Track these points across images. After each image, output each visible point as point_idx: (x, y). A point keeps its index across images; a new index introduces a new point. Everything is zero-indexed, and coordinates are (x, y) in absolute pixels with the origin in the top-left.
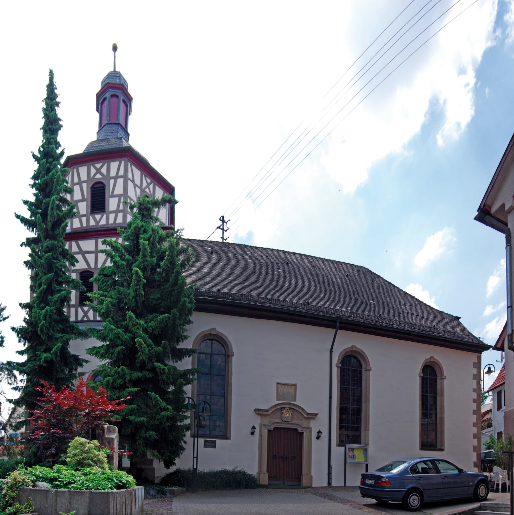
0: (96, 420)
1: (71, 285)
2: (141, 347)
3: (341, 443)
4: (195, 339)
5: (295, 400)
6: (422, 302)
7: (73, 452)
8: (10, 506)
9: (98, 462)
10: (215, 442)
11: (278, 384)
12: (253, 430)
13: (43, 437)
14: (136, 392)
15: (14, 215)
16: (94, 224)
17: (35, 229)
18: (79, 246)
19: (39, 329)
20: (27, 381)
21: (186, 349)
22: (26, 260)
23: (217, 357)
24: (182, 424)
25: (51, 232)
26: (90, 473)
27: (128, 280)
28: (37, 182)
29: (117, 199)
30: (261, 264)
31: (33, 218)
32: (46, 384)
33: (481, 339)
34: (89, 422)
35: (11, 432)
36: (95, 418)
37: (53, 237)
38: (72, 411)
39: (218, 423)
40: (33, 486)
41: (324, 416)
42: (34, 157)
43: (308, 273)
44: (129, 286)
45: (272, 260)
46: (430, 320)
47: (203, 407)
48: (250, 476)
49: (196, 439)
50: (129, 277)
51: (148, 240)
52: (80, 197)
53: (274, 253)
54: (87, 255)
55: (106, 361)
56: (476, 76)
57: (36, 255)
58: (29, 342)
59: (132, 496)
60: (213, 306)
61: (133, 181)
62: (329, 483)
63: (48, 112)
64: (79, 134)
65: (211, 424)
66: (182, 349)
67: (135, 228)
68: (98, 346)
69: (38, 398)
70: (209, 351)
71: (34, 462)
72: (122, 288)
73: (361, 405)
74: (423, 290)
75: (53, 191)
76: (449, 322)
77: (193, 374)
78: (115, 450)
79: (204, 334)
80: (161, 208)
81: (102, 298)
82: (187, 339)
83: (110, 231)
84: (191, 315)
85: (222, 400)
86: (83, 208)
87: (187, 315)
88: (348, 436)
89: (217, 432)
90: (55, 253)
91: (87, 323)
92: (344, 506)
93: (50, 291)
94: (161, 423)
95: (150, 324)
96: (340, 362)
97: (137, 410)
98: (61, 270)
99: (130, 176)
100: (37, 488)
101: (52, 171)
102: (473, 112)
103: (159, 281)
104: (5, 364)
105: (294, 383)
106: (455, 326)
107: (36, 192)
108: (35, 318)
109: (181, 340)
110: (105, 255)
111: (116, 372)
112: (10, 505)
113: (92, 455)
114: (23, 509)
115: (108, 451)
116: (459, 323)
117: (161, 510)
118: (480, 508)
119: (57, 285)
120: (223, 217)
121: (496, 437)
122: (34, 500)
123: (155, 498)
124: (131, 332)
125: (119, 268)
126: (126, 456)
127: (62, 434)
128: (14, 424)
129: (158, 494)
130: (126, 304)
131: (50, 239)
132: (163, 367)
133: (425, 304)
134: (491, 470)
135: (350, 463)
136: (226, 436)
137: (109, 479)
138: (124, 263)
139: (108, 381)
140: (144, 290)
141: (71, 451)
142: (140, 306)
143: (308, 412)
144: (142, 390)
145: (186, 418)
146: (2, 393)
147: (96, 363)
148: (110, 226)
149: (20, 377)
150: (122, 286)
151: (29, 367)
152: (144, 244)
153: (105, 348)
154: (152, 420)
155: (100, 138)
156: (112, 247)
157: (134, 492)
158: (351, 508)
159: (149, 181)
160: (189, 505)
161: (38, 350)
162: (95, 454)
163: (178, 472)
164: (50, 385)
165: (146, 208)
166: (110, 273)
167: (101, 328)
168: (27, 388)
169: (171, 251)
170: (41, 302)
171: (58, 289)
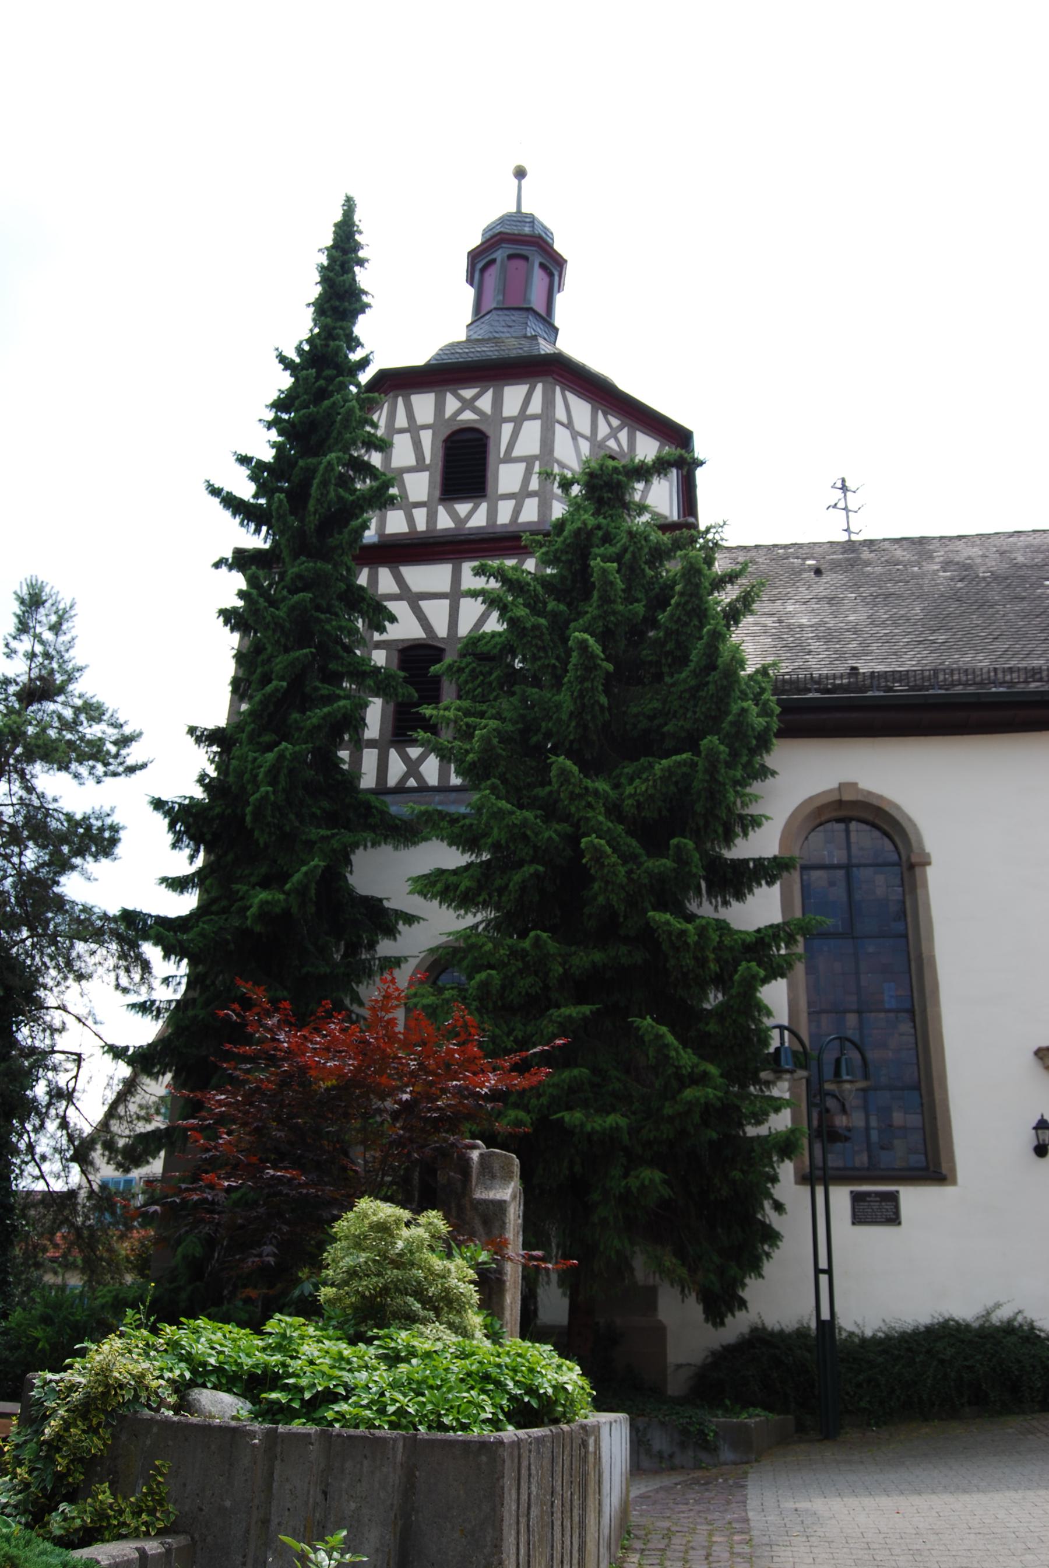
0: (437, 1130)
1: (370, 682)
2: (602, 865)
7: (348, 1262)
9: (443, 1305)
10: (893, 1198)
13: (235, 1196)
14: (585, 1018)
15: (204, 486)
17: (264, 529)
18: (400, 580)
19: (249, 810)
20: (189, 984)
21: (758, 862)
22: (228, 605)
24: (762, 1130)
25: (314, 540)
26: (412, 1353)
27: (554, 666)
28: (285, 416)
29: (522, 466)
30: (984, 578)
31: (262, 501)
34: (411, 1140)
35: (106, 1171)
36: (437, 1124)
38: (352, 1093)
39: (898, 1118)
40: (177, 1409)
44: (557, 684)
45: (1020, 559)
47: (838, 1061)
49: (820, 1190)
50: (558, 658)
51: (618, 558)
52: (412, 461)
54: (424, 604)
55: (479, 917)
58: (208, 852)
61: (569, 425)
63: (331, 274)
64: (417, 314)
65: (874, 1123)
66: (746, 861)
67: (577, 533)
69: (228, 1046)
70: (838, 856)
75: (331, 441)
77: (790, 940)
82: (759, 825)
84: (768, 750)
85: (906, 1027)
86: (419, 486)
87: (754, 752)
91: (415, 796)
93: (297, 695)
95: (629, 790)
98: (338, 641)
99: (560, 414)
100: (194, 1419)
104: (115, 919)
107: (280, 439)
108: (240, 775)
109: (738, 830)
110: (483, 602)
111: (514, 953)
113: (420, 1274)
114: (127, 1518)
115: (483, 1257)
119: (323, 681)
120: (843, 480)
123: (673, 1468)
124: (566, 818)
125: (525, 636)
126: (554, 1277)
127: (305, 1185)
130: (548, 735)
131: (310, 556)
132: (678, 925)
136: (933, 1168)
137: (486, 1378)
139: (485, 985)
140: (607, 692)
141: (341, 1257)
145: (777, 1105)
146: (90, 1022)
147: (440, 924)
148: (498, 530)
150: (537, 682)
151: (202, 934)
152: (604, 571)
159: (615, 422)
162: (430, 1270)
167: (463, 810)
169: (688, 582)
171: (325, 692)
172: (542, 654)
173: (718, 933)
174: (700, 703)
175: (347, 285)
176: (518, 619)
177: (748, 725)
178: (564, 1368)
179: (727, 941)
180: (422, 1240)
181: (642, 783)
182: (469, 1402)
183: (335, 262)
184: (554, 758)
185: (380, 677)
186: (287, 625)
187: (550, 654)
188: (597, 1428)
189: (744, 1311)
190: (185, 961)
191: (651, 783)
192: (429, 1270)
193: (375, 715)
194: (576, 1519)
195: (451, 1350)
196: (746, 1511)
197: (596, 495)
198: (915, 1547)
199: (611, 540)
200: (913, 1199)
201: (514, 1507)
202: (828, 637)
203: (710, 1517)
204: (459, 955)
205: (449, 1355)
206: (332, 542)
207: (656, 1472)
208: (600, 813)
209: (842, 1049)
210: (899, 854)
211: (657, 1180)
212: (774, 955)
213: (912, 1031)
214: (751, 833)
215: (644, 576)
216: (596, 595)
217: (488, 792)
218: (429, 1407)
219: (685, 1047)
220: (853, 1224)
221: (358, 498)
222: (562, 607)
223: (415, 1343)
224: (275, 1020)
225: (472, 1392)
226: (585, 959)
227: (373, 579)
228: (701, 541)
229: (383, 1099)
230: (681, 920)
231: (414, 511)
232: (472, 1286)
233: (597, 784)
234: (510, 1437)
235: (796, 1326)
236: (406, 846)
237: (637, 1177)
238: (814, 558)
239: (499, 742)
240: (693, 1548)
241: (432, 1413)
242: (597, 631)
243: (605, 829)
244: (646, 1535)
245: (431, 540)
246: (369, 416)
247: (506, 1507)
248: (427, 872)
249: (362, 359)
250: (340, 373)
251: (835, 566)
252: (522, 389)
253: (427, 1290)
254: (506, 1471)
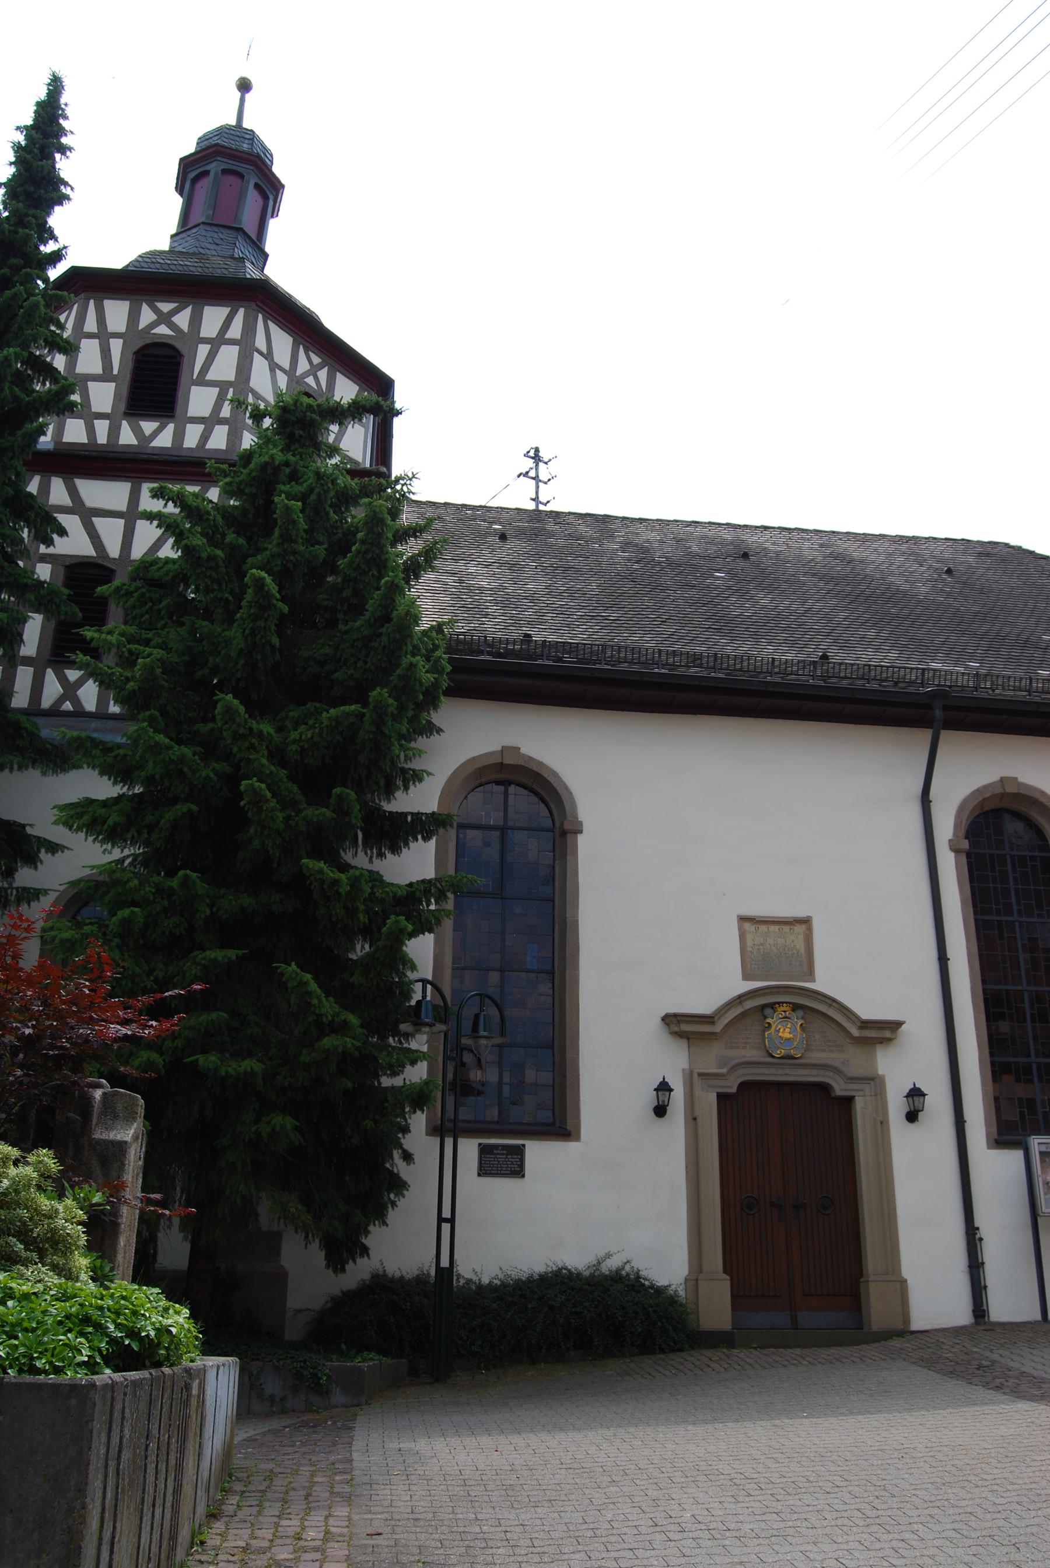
3: (1007, 1133)
5: (810, 975)
9: (49, 1247)
10: (520, 1151)
11: (742, 919)
21: (417, 816)
23: (525, 845)
24: (398, 1081)
27: (227, 601)
30: (660, 563)
39: (530, 1075)
43: (814, 575)
44: (229, 619)
45: (695, 548)
47: (477, 1017)
48: (660, 1291)
49: (449, 1142)
50: (231, 593)
51: (303, 498)
52: (98, 370)
55: (126, 852)
61: (268, 356)
62: (979, 1310)
63: (29, 157)
65: (506, 1079)
66: (404, 815)
67: (264, 467)
68: (102, 797)
70: (495, 818)
77: (441, 897)
78: (128, 1194)
82: (421, 780)
84: (436, 708)
85: (545, 988)
86: (103, 397)
88: (1031, 1104)
95: (294, 735)
96: (962, 833)
99: (260, 342)
101: (14, 286)
105: (802, 913)
109: (399, 783)
110: (159, 526)
113: (25, 1214)
115: (97, 1198)
120: (537, 450)
123: (284, 1412)
126: (176, 1221)
130: (215, 671)
132: (331, 874)
136: (560, 1125)
137: (86, 1320)
138: (219, 552)
139: (127, 923)
140: (280, 633)
145: (413, 1057)
147: (84, 856)
150: (208, 615)
152: (288, 508)
155: (180, 249)
159: (316, 360)
162: (37, 1211)
167: (120, 739)
172: (215, 587)
173: (370, 884)
174: (372, 653)
175: (46, 171)
176: (194, 548)
177: (415, 680)
178: (171, 1311)
179: (378, 893)
180: (31, 1179)
181: (308, 730)
182: (65, 1345)
183: (34, 144)
184: (221, 696)
185: (42, 592)
187: (224, 587)
188: (203, 1371)
189: (366, 1258)
191: (317, 731)
192: (36, 1210)
193: (33, 631)
195: (52, 1293)
196: (350, 1452)
197: (288, 430)
198: (509, 1482)
199: (299, 479)
200: (538, 1154)
201: (103, 1451)
202: (506, 602)
203: (314, 1458)
205: (48, 1297)
207: (267, 1416)
208: (263, 756)
209: (482, 1005)
210: (553, 820)
211: (289, 1127)
212: (423, 910)
213: (551, 992)
214: (412, 787)
215: (328, 519)
216: (277, 532)
217: (146, 724)
218: (22, 1350)
220: (479, 1175)
221: (34, 400)
222: (241, 541)
223: (14, 1285)
225: (69, 1335)
226: (234, 902)
227: (45, 489)
230: (335, 870)
232: (80, 1227)
233: (262, 726)
234: (103, 1379)
235: (416, 1272)
237: (269, 1123)
238: (500, 524)
239: (162, 673)
240: (294, 1489)
241: (25, 1356)
242: (275, 569)
243: (268, 772)
244: (248, 1477)
245: (111, 455)
246: (55, 315)
247: (94, 1450)
249: (53, 252)
250: (28, 263)
251: (520, 533)
252: (223, 312)
253: (32, 1230)
254: (96, 1414)
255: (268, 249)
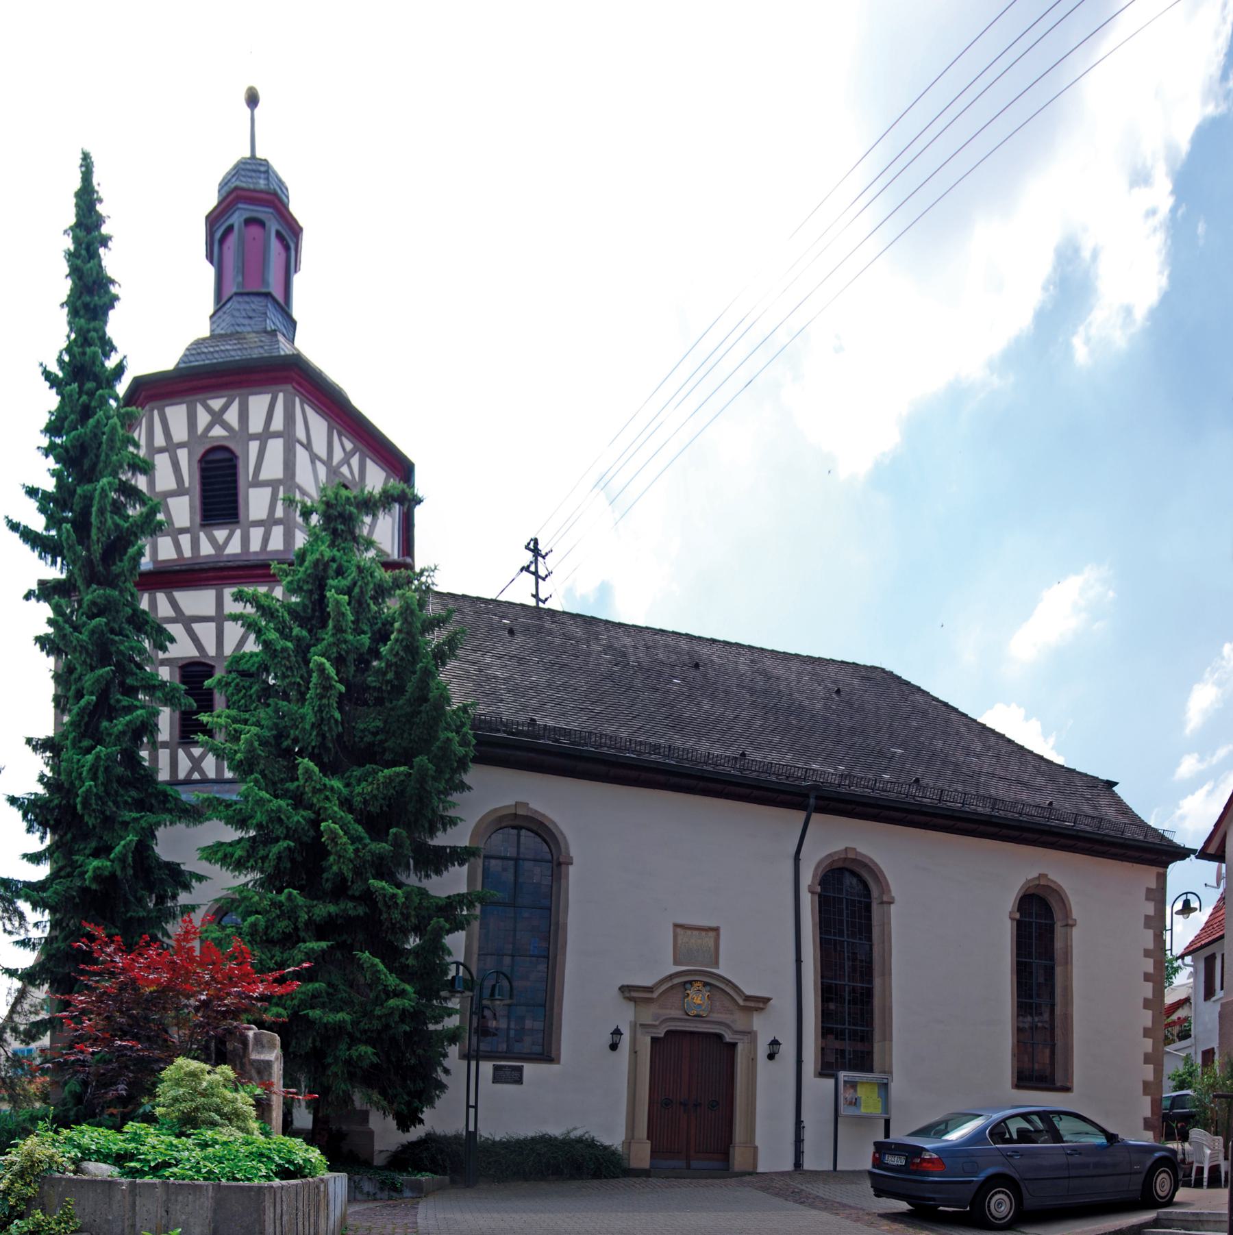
0: (225, 1018)
1: (159, 694)
2: (336, 844)
3: (826, 1069)
4: (476, 826)
5: (716, 963)
6: (1022, 748)
7: (172, 1093)
8: (20, 1217)
9: (234, 1117)
10: (520, 1069)
11: (676, 926)
12: (616, 1038)
13: (97, 1057)
14: (323, 951)
15: (4, 522)
16: (212, 552)
17: (59, 559)
18: (174, 604)
19: (79, 800)
21: (453, 849)
22: (42, 633)
23: (530, 877)
24: (439, 1027)
25: (101, 568)
26: (215, 1142)
27: (299, 684)
28: (58, 441)
29: (268, 490)
31: (53, 533)
32: (101, 933)
33: (1166, 834)
36: (224, 1015)
37: (109, 581)
38: (164, 996)
39: (528, 1024)
40: (75, 1172)
41: (784, 1004)
42: (46, 379)
43: (744, 687)
44: (302, 699)
45: (660, 656)
46: (1040, 790)
47: (494, 987)
48: (606, 1148)
49: (473, 1064)
50: (302, 677)
51: (348, 591)
52: (172, 485)
53: (664, 640)
54: (196, 627)
55: (249, 877)
56: (1173, 192)
57: (66, 622)
58: (53, 833)
59: (318, 1194)
60: (519, 753)
61: (308, 446)
62: (798, 1164)
63: (79, 262)
64: (164, 316)
65: (513, 1025)
66: (444, 848)
67: (316, 563)
68: (228, 840)
69: (82, 966)
70: (511, 852)
71: (76, 1115)
72: (285, 703)
73: (870, 981)
74: (1027, 718)
75: (101, 465)
76: (1087, 793)
77: (471, 906)
78: (275, 1089)
79: (499, 814)
80: (381, 515)
81: (237, 726)
82: (455, 824)
83: (251, 570)
84: (465, 771)
86: (181, 511)
87: (454, 771)
88: (843, 1052)
89: (527, 1045)
90: (114, 619)
91: (199, 786)
92: (833, 1217)
93: (104, 708)
94: (387, 1027)
95: (358, 789)
96: (817, 881)
97: (328, 994)
99: (300, 433)
102: (1163, 281)
103: (380, 690)
105: (713, 924)
106: (1104, 802)
107: (57, 466)
108: (69, 774)
109: (440, 826)
110: (243, 626)
111: (273, 904)
112: (21, 1217)
113: (218, 1100)
114: (53, 1226)
115: (258, 1091)
116: (1114, 795)
117: (390, 1227)
118: (1156, 1223)
119: (123, 694)
120: (536, 541)
121: (1199, 1061)
122: (77, 1204)
124: (310, 807)
125: (276, 656)
126: (303, 1104)
127: (141, 1050)
128: (22, 1028)
129: (382, 1189)
130: (296, 741)
131: (99, 584)
132: (391, 890)
133: (1031, 752)
134: (1184, 1137)
135: (847, 1116)
136: (547, 1055)
137: (262, 1155)
138: (289, 644)
139: (254, 925)
140: (340, 709)
141: (166, 1092)
142: (331, 745)
143: (748, 993)
144: (340, 946)
145: (450, 1013)
147: (222, 882)
149: (32, 916)
150: (286, 697)
151: (56, 893)
152: (338, 602)
153: (246, 845)
154: (365, 1020)
155: (219, 331)
156: (260, 607)
157: (322, 1186)
158: (848, 1222)
159: (349, 446)
160: (458, 1216)
161: (78, 852)
162: (225, 1098)
163: (429, 1140)
164: (110, 936)
165: (341, 515)
166: (254, 669)
167: (234, 798)
168: (52, 943)
169: (405, 621)
170: (83, 736)
171: (125, 703)
184: (300, 760)
186: (90, 647)
190: (47, 911)
193: (165, 719)
194: (312, 1221)
204: (236, 904)
206: (115, 569)
219: (391, 973)
224: (112, 948)
227: (153, 604)
228: (416, 582)
229: (188, 999)
231: (180, 537)
236: (195, 824)
245: (197, 567)
248: (211, 844)
251: (525, 629)
255: (296, 313)
